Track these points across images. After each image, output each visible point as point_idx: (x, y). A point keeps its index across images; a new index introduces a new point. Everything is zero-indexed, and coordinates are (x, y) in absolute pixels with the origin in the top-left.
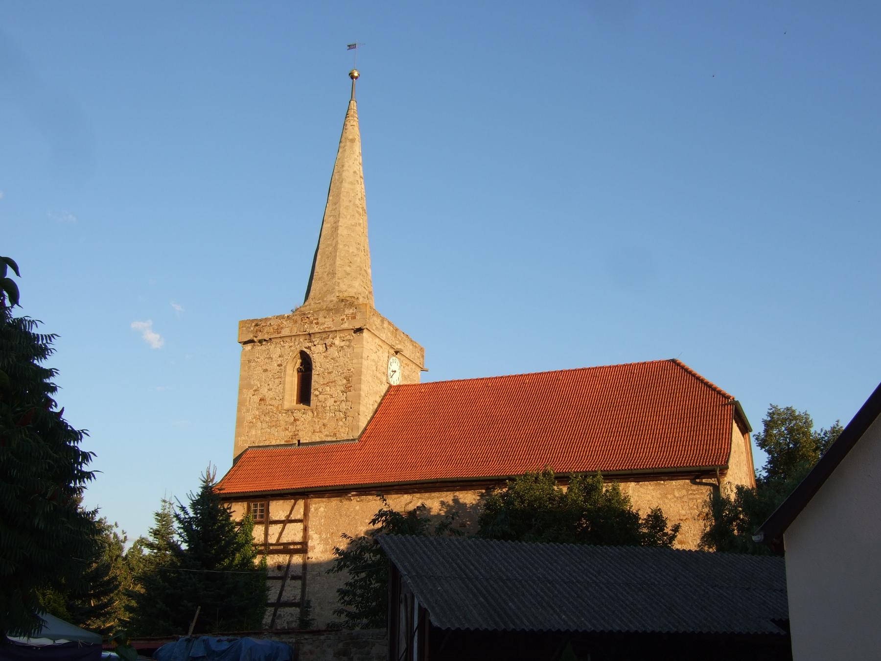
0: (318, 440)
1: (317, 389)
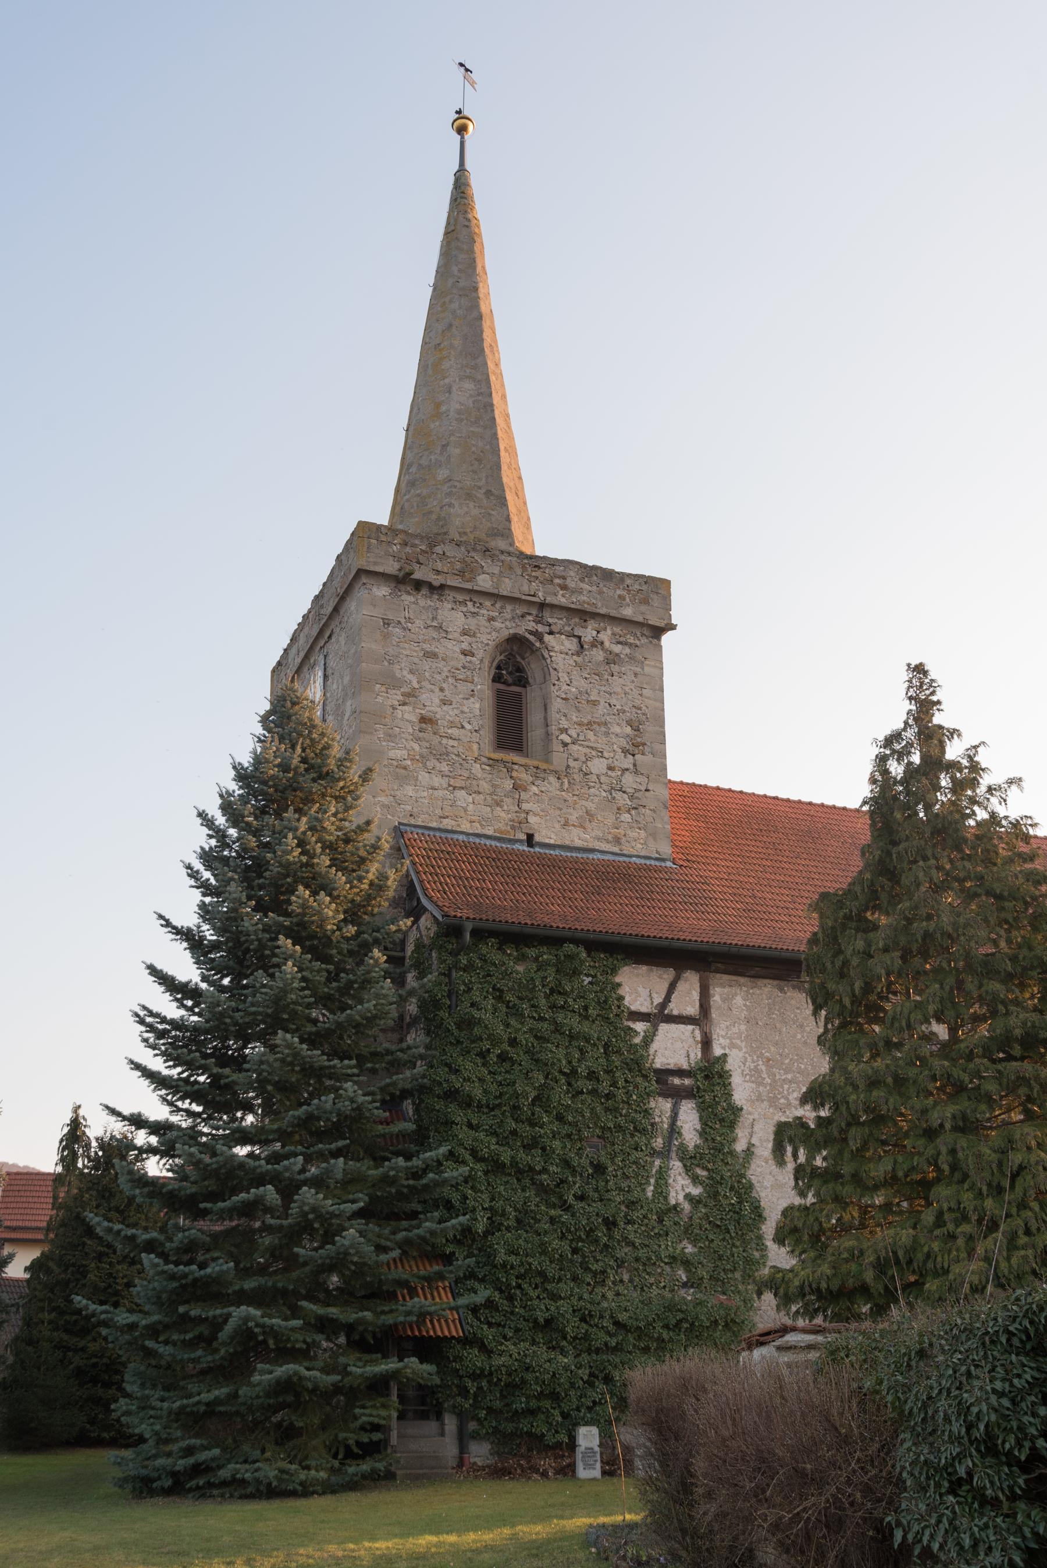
0: (578, 843)
1: (565, 731)
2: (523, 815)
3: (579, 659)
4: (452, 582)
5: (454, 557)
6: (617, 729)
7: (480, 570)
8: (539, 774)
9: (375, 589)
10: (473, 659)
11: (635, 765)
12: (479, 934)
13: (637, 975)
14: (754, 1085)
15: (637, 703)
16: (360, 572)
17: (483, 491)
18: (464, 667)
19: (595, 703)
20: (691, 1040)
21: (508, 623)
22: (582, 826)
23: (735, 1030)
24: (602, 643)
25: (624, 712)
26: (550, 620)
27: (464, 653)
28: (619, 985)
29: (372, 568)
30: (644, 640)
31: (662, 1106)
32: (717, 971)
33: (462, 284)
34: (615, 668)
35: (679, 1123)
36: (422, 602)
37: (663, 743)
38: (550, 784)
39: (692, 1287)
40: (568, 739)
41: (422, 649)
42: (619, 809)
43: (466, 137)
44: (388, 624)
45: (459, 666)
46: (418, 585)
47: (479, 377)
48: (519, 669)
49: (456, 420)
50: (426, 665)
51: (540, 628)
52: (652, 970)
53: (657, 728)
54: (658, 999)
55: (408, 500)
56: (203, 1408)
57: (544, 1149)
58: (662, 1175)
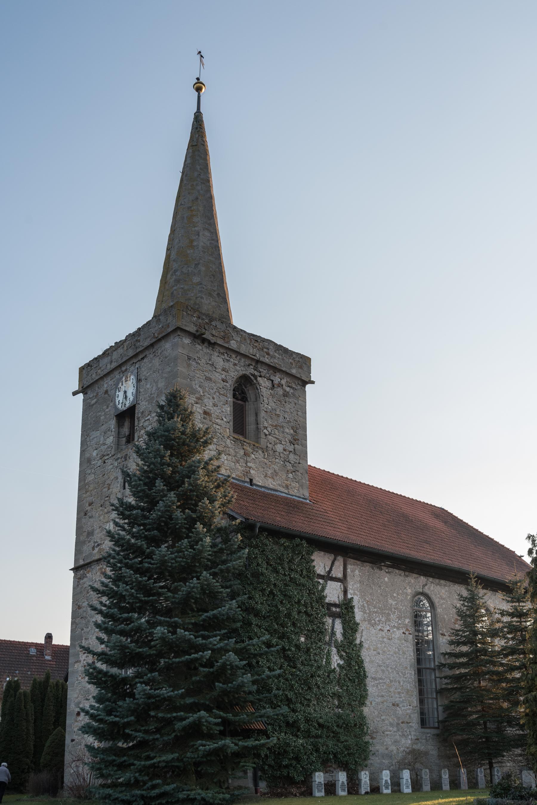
0: (271, 486)
1: (266, 428)
2: (248, 469)
3: (272, 392)
4: (220, 342)
5: (221, 329)
6: (287, 430)
7: (231, 338)
8: (255, 448)
9: (184, 339)
10: (227, 384)
11: (294, 450)
12: (263, 529)
13: (320, 556)
14: (362, 613)
15: (296, 418)
16: (178, 329)
17: (216, 293)
18: (223, 388)
19: (278, 416)
20: (340, 590)
21: (242, 368)
22: (273, 478)
23: (355, 586)
24: (282, 385)
25: (290, 422)
26: (261, 370)
27: (223, 381)
28: (313, 561)
29: (184, 328)
30: (299, 387)
31: (329, 621)
32: (349, 558)
33: (202, 177)
34: (287, 399)
35: (335, 630)
36: (205, 350)
37: (306, 440)
38: (260, 454)
39: (340, 708)
40: (267, 433)
41: (205, 375)
42: (288, 471)
43: (201, 93)
44: (190, 359)
45: (221, 387)
46: (204, 341)
47: (212, 231)
48: (243, 392)
49: (202, 251)
50: (206, 384)
51: (256, 373)
52: (325, 554)
53: (303, 432)
54: (327, 569)
55: (175, 290)
56: (164, 764)
57: (288, 638)
58: (329, 654)
